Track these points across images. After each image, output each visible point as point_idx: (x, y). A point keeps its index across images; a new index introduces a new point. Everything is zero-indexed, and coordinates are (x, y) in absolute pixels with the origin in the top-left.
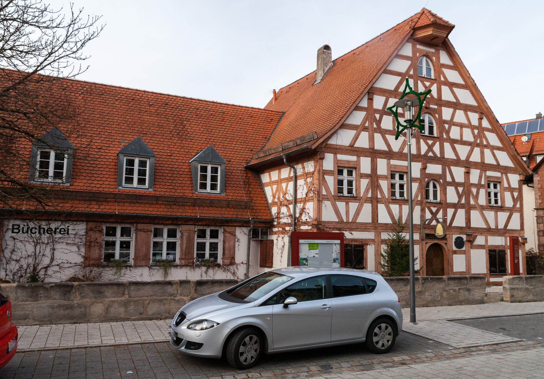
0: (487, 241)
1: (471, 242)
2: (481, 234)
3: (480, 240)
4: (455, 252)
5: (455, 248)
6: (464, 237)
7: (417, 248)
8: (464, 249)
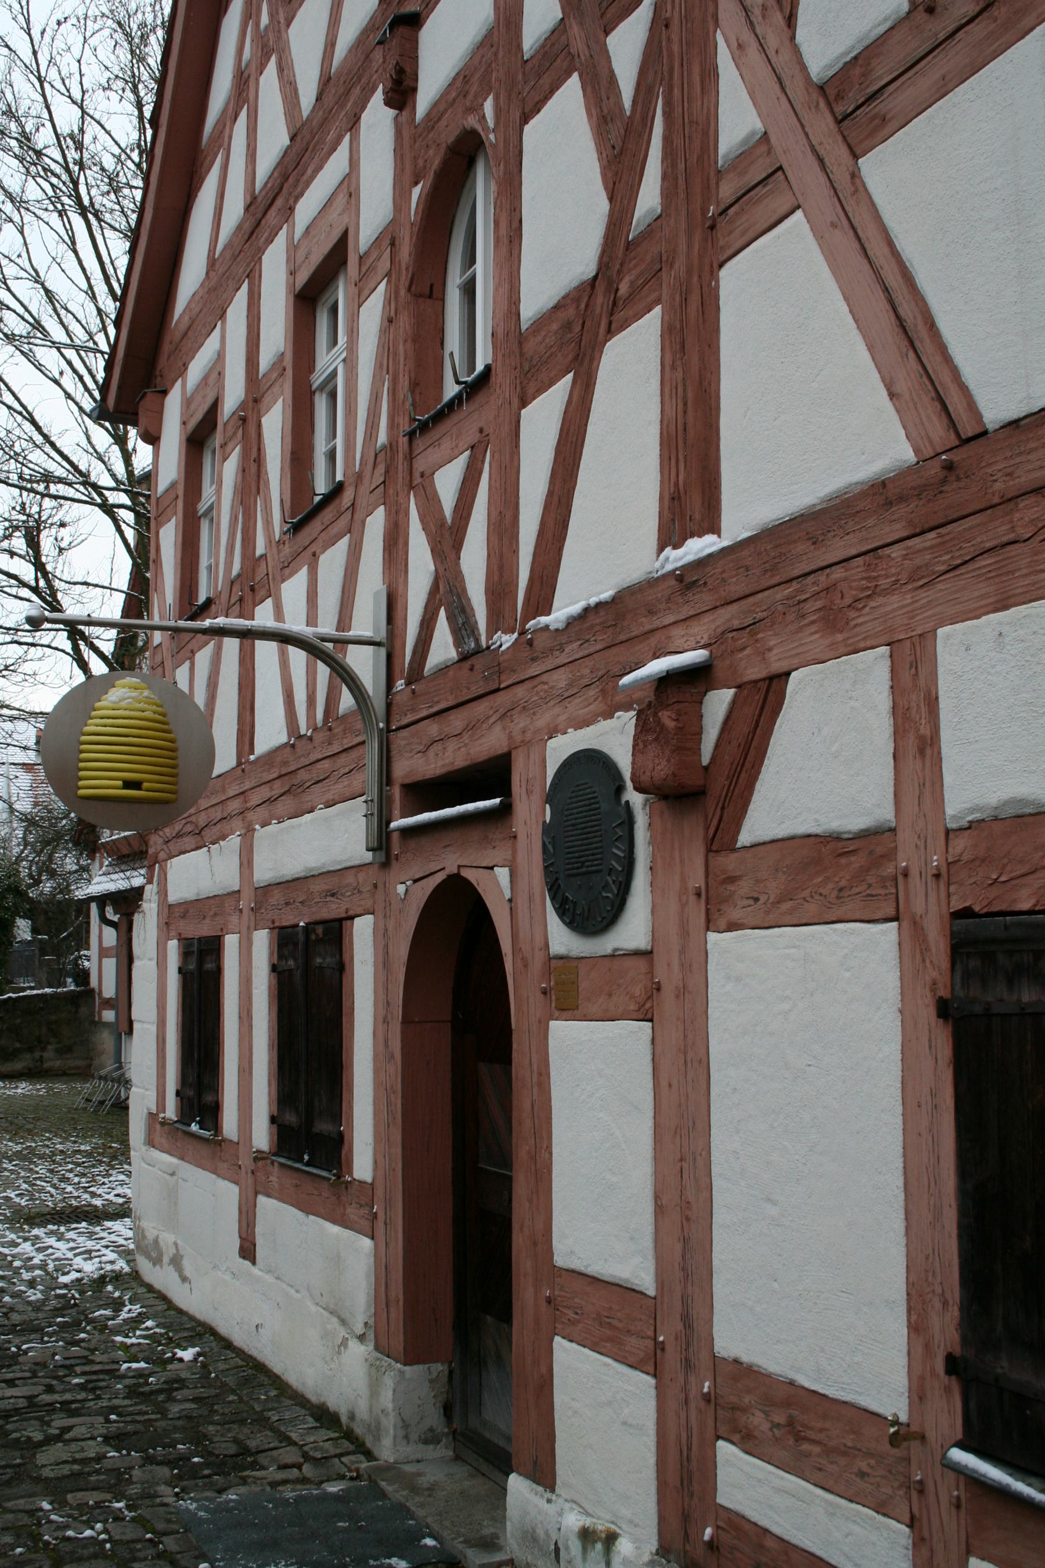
0: (916, 733)
1: (706, 792)
2: (839, 629)
3: (824, 761)
4: (569, 992)
5: (561, 939)
6: (615, 737)
7: (363, 931)
8: (634, 929)
